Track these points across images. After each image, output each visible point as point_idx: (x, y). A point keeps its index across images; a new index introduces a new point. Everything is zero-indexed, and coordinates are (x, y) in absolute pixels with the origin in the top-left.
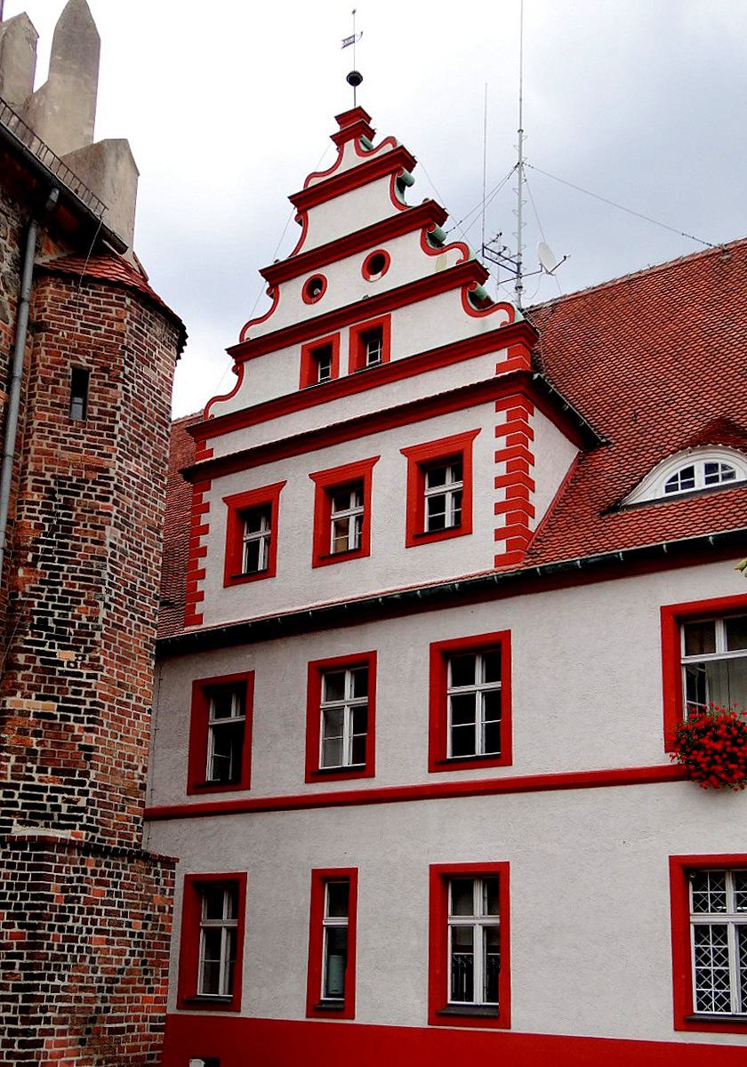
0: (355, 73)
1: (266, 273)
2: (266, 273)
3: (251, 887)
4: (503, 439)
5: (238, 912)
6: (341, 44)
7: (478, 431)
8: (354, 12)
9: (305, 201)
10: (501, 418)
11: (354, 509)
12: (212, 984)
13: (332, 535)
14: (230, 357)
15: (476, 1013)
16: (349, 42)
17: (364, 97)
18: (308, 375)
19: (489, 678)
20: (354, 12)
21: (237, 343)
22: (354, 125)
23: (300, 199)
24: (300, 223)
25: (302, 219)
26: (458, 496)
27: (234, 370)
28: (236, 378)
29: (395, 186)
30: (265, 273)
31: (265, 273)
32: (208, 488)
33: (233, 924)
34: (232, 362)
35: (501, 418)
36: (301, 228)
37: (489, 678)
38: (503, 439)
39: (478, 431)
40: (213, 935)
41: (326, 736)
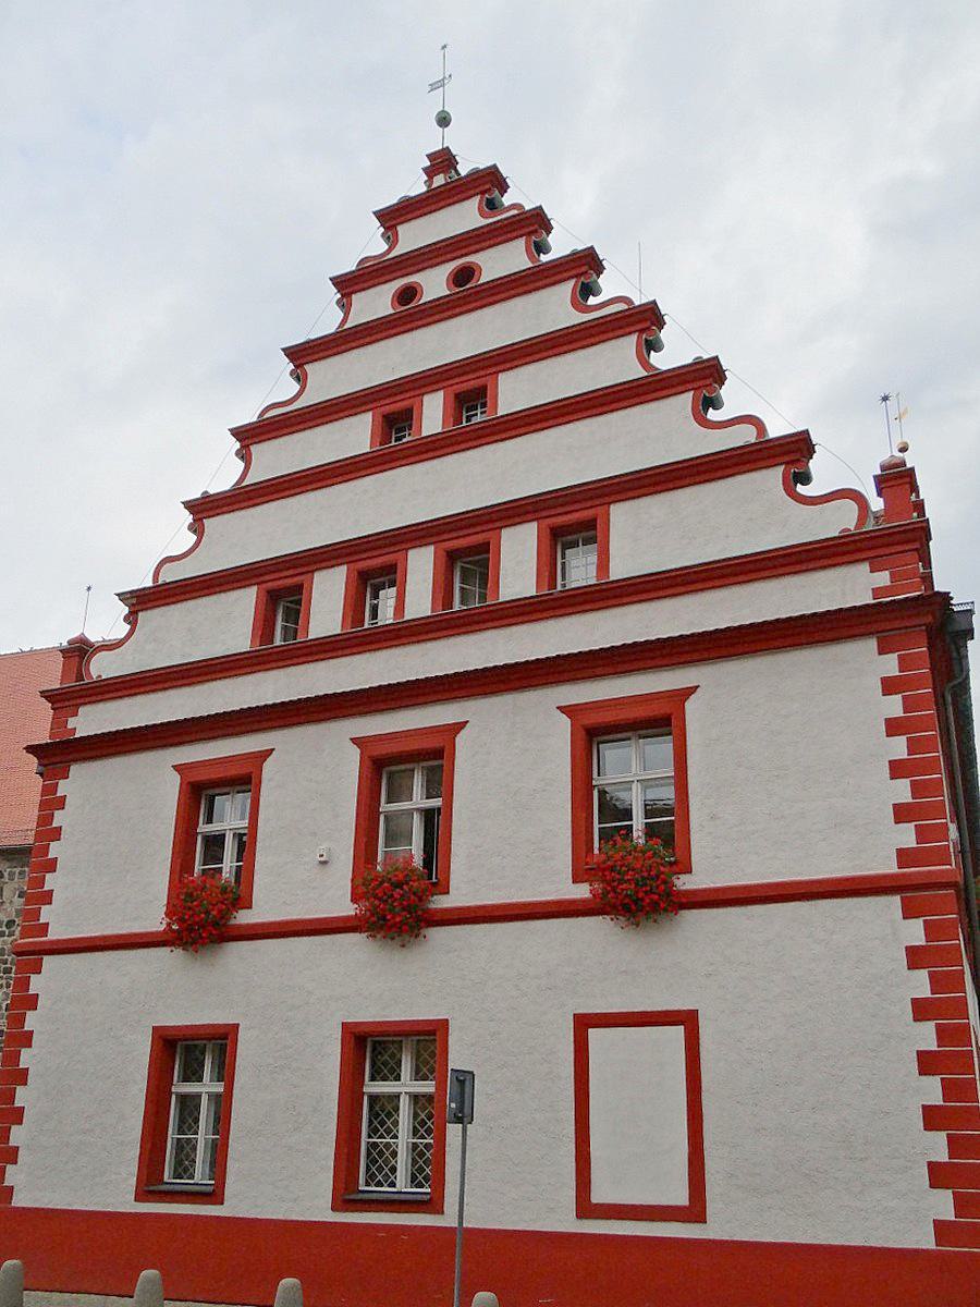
1: (191, 506)
2: (191, 506)
3: (244, 1038)
5: (226, 1072)
8: (89, 589)
9: (249, 436)
11: (208, 1087)
12: (183, 1167)
13: (170, 1129)
15: (466, 1096)
17: (454, 140)
18: (264, 628)
19: (419, 1075)
20: (89, 589)
21: (149, 583)
22: (442, 161)
23: (292, 353)
24: (242, 458)
26: (429, 816)
29: (467, 287)
30: (189, 505)
31: (189, 505)
33: (219, 1088)
34: (190, 518)
36: (243, 465)
40: (189, 1104)
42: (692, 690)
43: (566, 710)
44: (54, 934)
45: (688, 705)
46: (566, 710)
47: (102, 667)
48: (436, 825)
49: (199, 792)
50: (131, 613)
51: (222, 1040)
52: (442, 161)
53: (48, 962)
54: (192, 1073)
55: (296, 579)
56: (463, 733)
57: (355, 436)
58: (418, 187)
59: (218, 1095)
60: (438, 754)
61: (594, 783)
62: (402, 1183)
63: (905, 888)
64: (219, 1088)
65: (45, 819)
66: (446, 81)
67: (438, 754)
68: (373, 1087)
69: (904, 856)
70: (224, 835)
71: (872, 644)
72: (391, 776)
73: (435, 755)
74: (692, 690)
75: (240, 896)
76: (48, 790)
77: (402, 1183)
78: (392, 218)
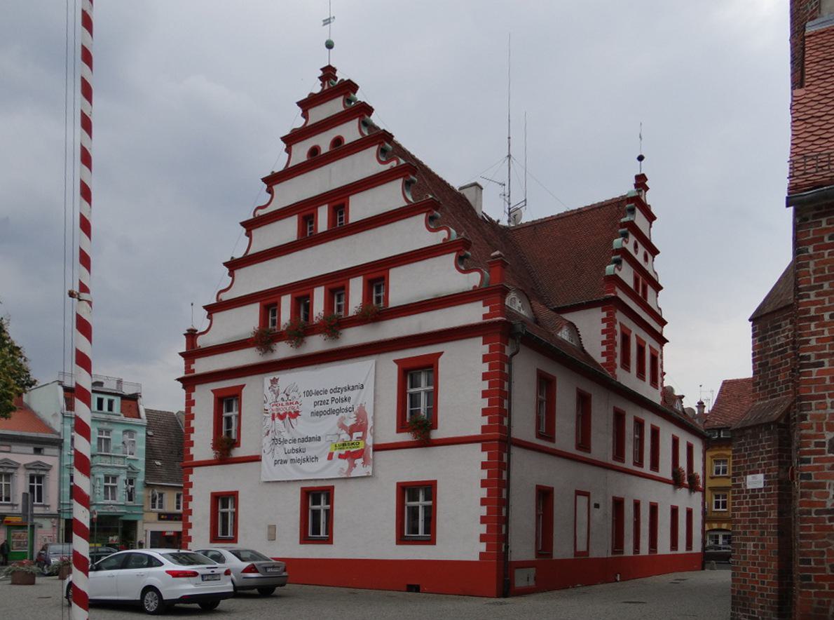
0: (333, 43)
1: (265, 180)
2: (265, 180)
4: (605, 336)
5: (236, 505)
6: (322, 23)
7: (442, 352)
9: (250, 226)
10: (604, 315)
11: (323, 506)
14: (282, 143)
16: (327, 22)
19: (426, 499)
21: (252, 217)
24: (288, 152)
25: (288, 150)
27: (208, 317)
28: (248, 238)
31: (226, 264)
32: (194, 363)
33: (234, 510)
35: (604, 315)
37: (426, 499)
38: (605, 336)
39: (442, 352)
41: (411, 407)
42: (441, 353)
43: (396, 361)
44: (196, 459)
45: (243, 391)
46: (396, 361)
47: (202, 342)
48: (433, 397)
49: (408, 372)
50: (209, 314)
51: (234, 495)
52: (328, 73)
53: (195, 470)
54: (317, 502)
55: (342, 283)
56: (441, 357)
57: (288, 230)
58: (317, 88)
59: (234, 513)
60: (431, 366)
61: (408, 391)
62: (421, 533)
63: (92, 467)
64: (234, 510)
65: (188, 410)
66: (331, 20)
67: (431, 366)
68: (312, 507)
69: (484, 428)
70: (420, 394)
71: (480, 339)
72: (412, 375)
73: (430, 366)
74: (441, 353)
75: (432, 423)
76: (188, 397)
77: (421, 533)
78: (306, 105)
